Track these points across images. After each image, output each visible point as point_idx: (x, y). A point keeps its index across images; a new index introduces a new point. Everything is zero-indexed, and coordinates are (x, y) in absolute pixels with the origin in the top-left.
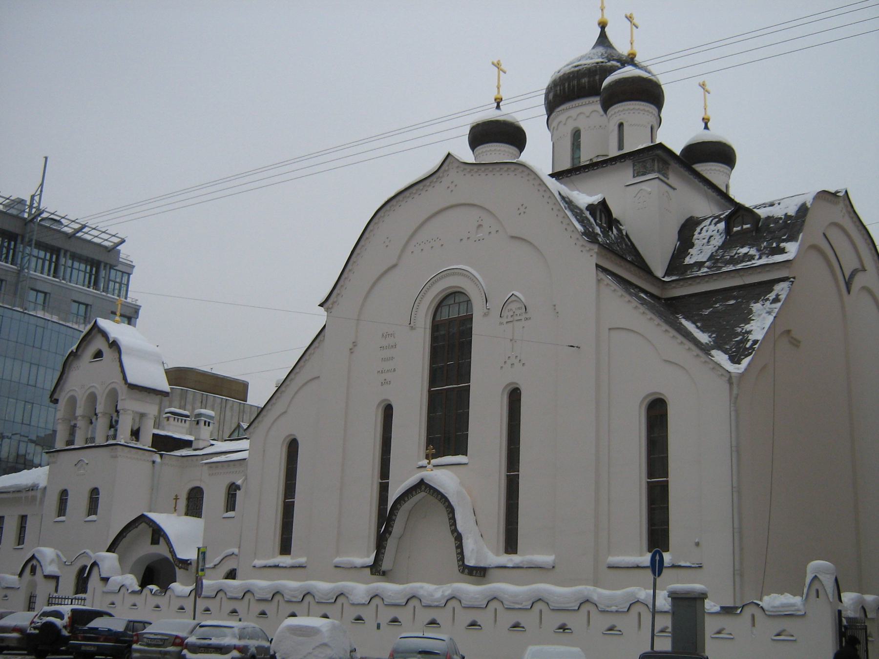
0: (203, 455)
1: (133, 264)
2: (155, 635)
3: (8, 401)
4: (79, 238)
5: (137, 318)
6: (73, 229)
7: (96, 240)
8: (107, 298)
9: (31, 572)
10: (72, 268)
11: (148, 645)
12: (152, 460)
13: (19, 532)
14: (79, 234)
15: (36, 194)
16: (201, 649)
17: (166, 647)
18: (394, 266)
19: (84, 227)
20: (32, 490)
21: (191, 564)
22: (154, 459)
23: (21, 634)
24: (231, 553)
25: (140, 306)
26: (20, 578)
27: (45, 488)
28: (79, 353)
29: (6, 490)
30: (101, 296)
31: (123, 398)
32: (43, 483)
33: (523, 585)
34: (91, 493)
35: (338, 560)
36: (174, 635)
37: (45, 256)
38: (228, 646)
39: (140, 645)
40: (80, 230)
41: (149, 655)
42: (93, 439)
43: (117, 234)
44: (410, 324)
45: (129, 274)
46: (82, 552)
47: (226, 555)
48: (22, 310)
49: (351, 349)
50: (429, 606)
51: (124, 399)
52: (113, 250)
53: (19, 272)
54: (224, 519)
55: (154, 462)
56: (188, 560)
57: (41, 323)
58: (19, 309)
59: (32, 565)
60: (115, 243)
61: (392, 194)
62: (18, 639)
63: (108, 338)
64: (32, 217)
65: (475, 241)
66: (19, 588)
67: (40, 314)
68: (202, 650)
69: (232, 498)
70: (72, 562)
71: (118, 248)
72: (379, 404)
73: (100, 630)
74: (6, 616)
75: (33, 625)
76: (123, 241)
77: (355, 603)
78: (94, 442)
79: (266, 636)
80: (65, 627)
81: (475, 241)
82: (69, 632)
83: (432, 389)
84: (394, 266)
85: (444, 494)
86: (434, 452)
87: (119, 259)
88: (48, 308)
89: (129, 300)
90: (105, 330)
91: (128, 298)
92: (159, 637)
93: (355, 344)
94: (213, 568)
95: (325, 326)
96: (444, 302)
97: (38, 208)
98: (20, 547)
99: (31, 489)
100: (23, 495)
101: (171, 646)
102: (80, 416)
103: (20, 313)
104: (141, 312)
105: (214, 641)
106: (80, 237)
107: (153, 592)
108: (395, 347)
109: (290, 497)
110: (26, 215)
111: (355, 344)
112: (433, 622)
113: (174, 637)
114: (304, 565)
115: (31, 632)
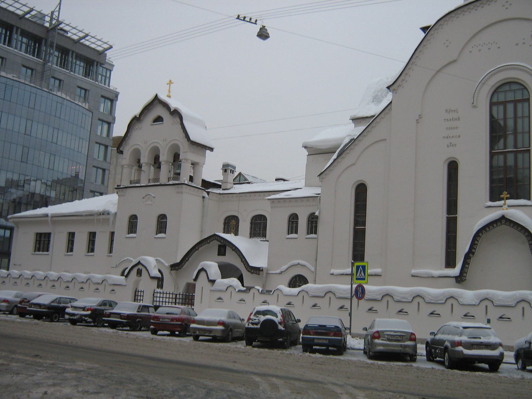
0: (239, 193)
1: (113, 64)
2: (394, 332)
3: (40, 152)
4: (82, 44)
5: (117, 100)
6: (85, 34)
7: (93, 46)
8: (99, 86)
9: (137, 274)
10: (76, 64)
11: (389, 340)
12: (202, 196)
13: (110, 244)
14: (82, 41)
15: (55, 11)
16: (474, 346)
17: (405, 342)
18: (455, 61)
19: (87, 35)
20: (103, 214)
21: (262, 270)
22: (204, 195)
23: (224, 327)
24: (297, 264)
25: (119, 93)
26: (126, 278)
27: (116, 213)
28: (141, 118)
29: (79, 214)
30: (95, 84)
31: (185, 151)
32: (113, 209)
33: (509, 291)
34: (130, 218)
35: (413, 271)
36: (410, 333)
37: (59, 55)
38: (495, 343)
39: (382, 340)
40: (84, 38)
41: (392, 348)
42: (157, 179)
43: (108, 42)
44: (473, 103)
45: (111, 71)
46: (125, 259)
47: (292, 265)
48: (48, 91)
49: (417, 120)
50: (463, 305)
51: (187, 152)
52: (102, 54)
53: (44, 65)
54: (308, 239)
55: (204, 197)
56: (260, 268)
57: (60, 100)
58: (46, 90)
59: (138, 270)
60: (104, 48)
61: (452, 8)
62: (223, 331)
63: (170, 108)
64: (52, 26)
65: (517, 44)
66: (126, 285)
67: (59, 94)
68: (475, 347)
69: (131, 224)
70: (116, 266)
71: (106, 52)
72: (445, 162)
73: (328, 327)
74: (238, 316)
75: (250, 321)
76: (111, 47)
77: (465, 304)
78: (179, 180)
79: (195, 313)
80: (280, 323)
81: (517, 44)
82: (283, 327)
83: (493, 151)
84: (455, 61)
85: (525, 227)
86: (509, 197)
87: (106, 60)
88: (62, 89)
89: (111, 88)
90: (166, 102)
91: (111, 87)
92: (399, 334)
93: (420, 116)
94: (280, 273)
95: (391, 102)
96: (498, 90)
97: (58, 20)
98: (69, 253)
99: (102, 213)
100: (96, 217)
101: (408, 341)
102: (127, 165)
103: (47, 93)
104: (119, 97)
105: (483, 340)
106: (82, 43)
107: (260, 292)
108: (459, 120)
109: (358, 225)
110: (47, 25)
111: (420, 117)
112: (264, 302)
113: (410, 334)
114: (380, 274)
115: (249, 326)
